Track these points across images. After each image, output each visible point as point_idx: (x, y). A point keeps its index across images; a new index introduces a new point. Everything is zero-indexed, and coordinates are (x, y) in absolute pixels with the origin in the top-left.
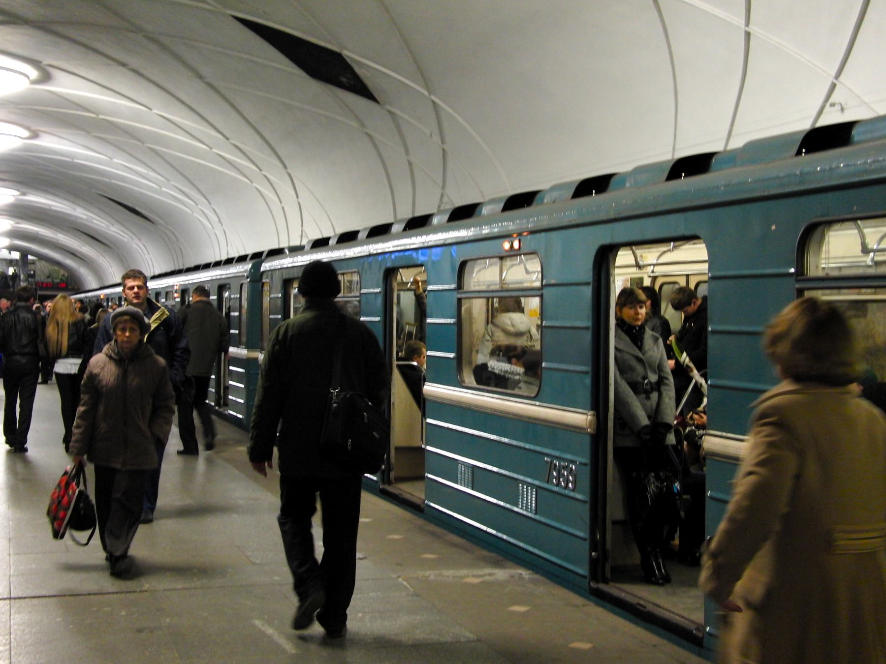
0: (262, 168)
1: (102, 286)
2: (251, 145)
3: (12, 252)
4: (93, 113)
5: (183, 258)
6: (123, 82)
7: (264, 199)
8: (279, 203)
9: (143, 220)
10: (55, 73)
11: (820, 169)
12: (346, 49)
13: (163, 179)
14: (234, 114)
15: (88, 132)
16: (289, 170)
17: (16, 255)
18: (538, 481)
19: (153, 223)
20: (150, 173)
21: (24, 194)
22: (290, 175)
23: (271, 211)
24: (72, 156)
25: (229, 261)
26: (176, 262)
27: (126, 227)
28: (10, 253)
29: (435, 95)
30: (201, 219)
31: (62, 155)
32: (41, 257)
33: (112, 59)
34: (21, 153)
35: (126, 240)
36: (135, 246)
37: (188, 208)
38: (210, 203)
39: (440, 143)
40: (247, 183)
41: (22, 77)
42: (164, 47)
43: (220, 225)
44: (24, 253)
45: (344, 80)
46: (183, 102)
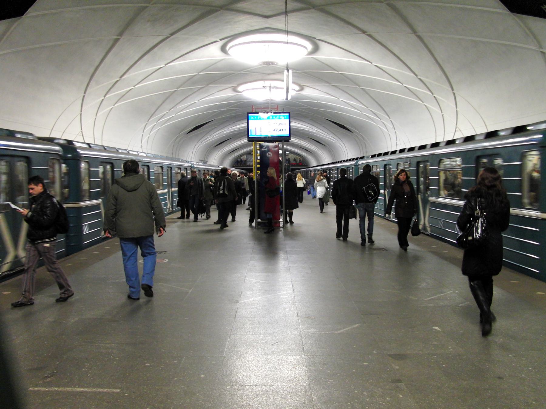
1: (319, 165)
5: (366, 148)
10: (322, 45)
11: (31, 215)
13: (365, 107)
16: (454, 91)
19: (352, 132)
22: (454, 94)
23: (432, 118)
24: (300, 127)
25: (350, 160)
26: (362, 150)
27: (316, 146)
31: (297, 127)
38: (390, 118)
46: (394, 54)
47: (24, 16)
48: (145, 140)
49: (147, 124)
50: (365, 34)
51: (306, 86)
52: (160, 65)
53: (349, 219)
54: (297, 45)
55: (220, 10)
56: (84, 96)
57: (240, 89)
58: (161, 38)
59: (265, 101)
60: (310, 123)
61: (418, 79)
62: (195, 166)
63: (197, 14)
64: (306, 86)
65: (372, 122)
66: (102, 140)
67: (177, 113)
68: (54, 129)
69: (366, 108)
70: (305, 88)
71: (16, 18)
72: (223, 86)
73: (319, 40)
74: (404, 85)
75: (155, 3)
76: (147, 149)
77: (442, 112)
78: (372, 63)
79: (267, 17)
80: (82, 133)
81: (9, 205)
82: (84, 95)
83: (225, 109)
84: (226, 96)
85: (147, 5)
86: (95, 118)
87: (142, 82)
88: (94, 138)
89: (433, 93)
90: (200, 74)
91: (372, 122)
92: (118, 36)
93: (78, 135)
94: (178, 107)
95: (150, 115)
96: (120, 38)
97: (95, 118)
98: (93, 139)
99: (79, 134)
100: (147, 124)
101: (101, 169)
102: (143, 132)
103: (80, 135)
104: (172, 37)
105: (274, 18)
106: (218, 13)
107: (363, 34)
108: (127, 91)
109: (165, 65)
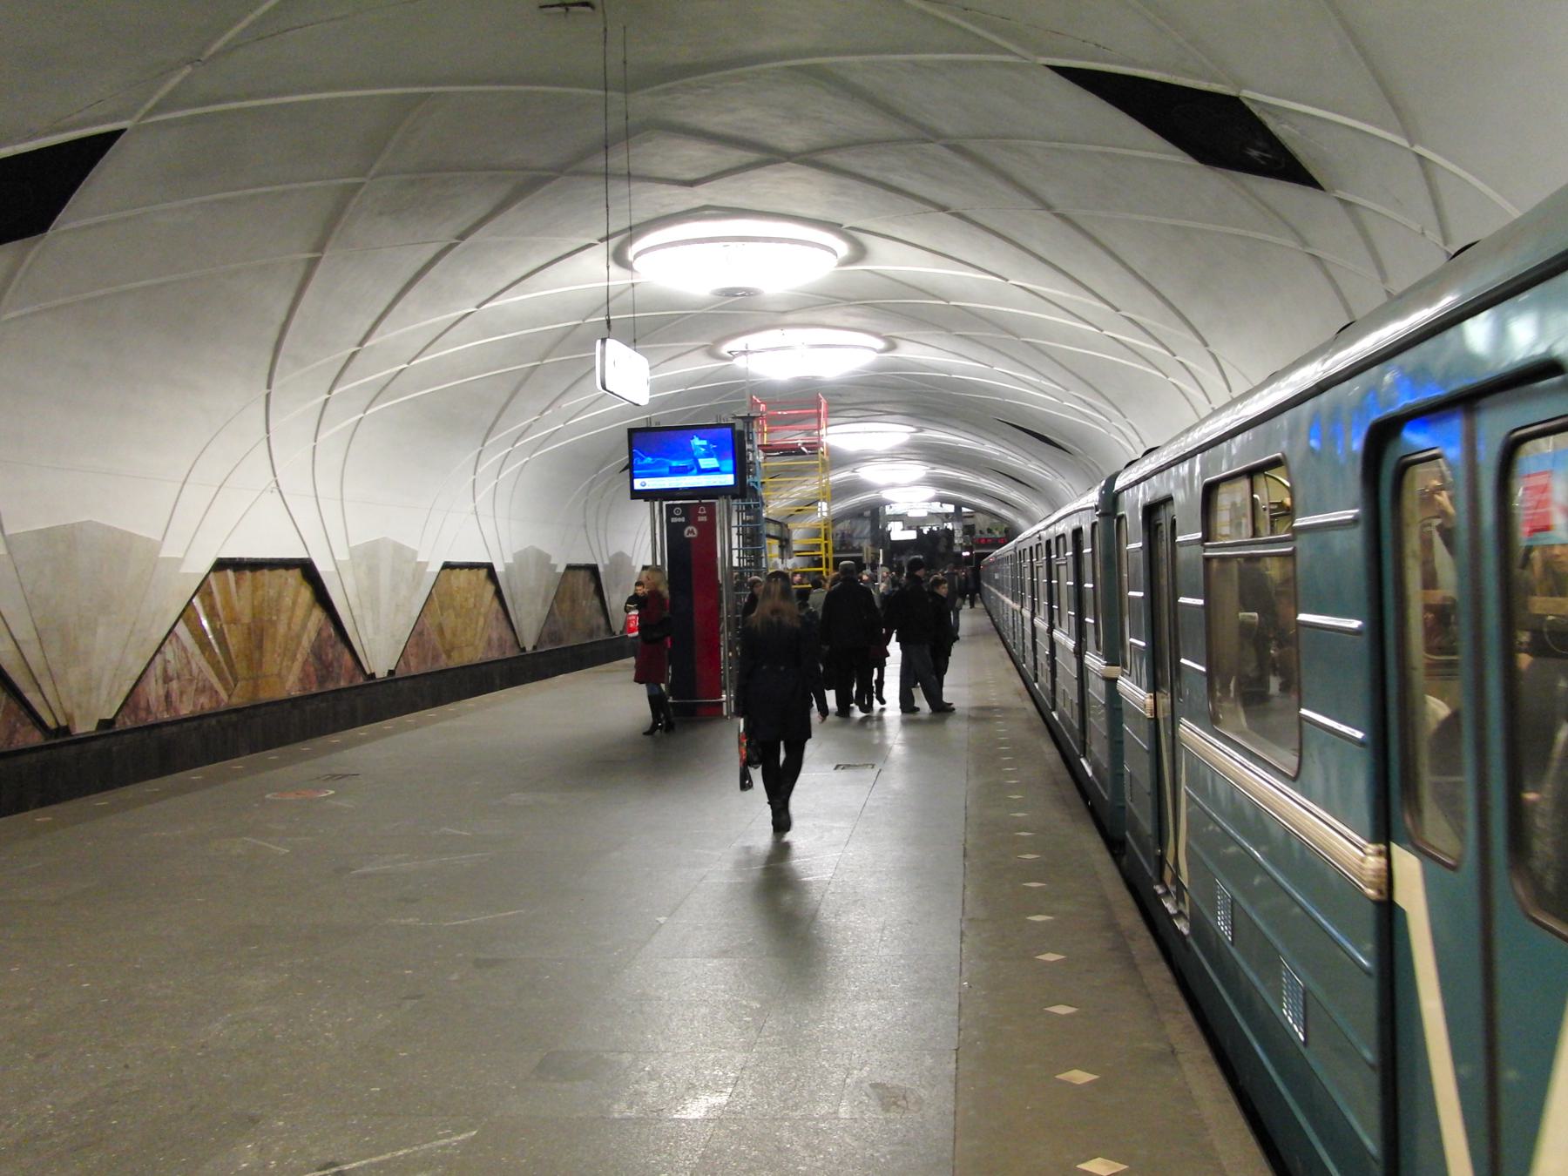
3: (943, 505)
4: (941, 299)
6: (957, 240)
8: (1207, 402)
9: (1056, 449)
12: (1245, 88)
14: (1116, 266)
15: (949, 331)
17: (950, 508)
21: (920, 430)
22: (1213, 355)
29: (1423, 144)
30: (1121, 442)
32: (978, 509)
34: (873, 373)
36: (1061, 486)
37: (1101, 426)
38: (1125, 417)
39: (1441, 245)
40: (1161, 378)
41: (817, 251)
45: (1254, 153)
47: (49, 232)
49: (480, 453)
50: (948, 214)
53: (826, 691)
55: (558, 177)
56: (268, 396)
57: (725, 349)
61: (1122, 319)
63: (503, 190)
65: (1095, 427)
66: (316, 496)
69: (1064, 391)
70: (902, 344)
73: (851, 228)
74: (1105, 332)
76: (494, 517)
77: (1210, 402)
79: (691, 183)
80: (278, 485)
81: (916, 559)
82: (267, 391)
83: (714, 403)
86: (314, 447)
89: (1176, 352)
91: (1095, 427)
92: (315, 251)
93: (264, 490)
94: (564, 406)
96: (321, 258)
97: (314, 447)
99: (269, 488)
100: (480, 453)
102: (475, 474)
103: (272, 492)
104: (463, 244)
105: (708, 184)
109: (478, 307)
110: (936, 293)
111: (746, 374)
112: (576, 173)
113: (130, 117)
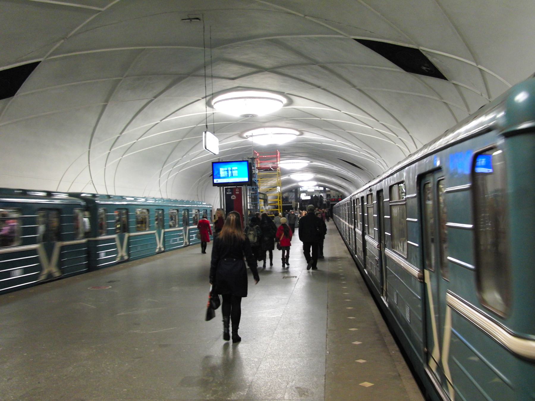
0: (398, 135)
2: (389, 122)
3: (320, 187)
4: (319, 118)
6: (324, 98)
7: (403, 151)
14: (371, 101)
15: (321, 128)
16: (410, 134)
17: (322, 189)
18: (491, 114)
20: (353, 146)
21: (312, 162)
24: (324, 166)
27: (346, 183)
28: (319, 188)
29: (481, 65)
32: (331, 189)
33: (312, 84)
35: (356, 178)
39: (488, 99)
40: (393, 144)
42: (332, 71)
43: (387, 167)
44: (325, 187)
47: (15, 96)
48: (163, 184)
49: (161, 170)
51: (304, 131)
52: (156, 121)
54: (270, 99)
57: (245, 135)
58: (145, 101)
59: (296, 142)
60: (321, 162)
62: (357, 196)
64: (304, 131)
66: (106, 186)
67: (192, 159)
68: (62, 180)
71: (12, 97)
72: (227, 134)
75: (127, 76)
78: (341, 111)
82: (89, 150)
83: (241, 153)
84: (235, 142)
85: (120, 78)
87: (144, 136)
88: (106, 186)
90: (198, 125)
92: (105, 102)
95: (163, 163)
98: (105, 186)
99: (90, 183)
100: (161, 170)
101: (116, 213)
102: (160, 177)
104: (156, 99)
106: (188, 79)
107: (318, 89)
108: (132, 144)
109: (161, 121)
110: (316, 115)
111: (252, 143)
112: (192, 76)
113: (42, 58)
